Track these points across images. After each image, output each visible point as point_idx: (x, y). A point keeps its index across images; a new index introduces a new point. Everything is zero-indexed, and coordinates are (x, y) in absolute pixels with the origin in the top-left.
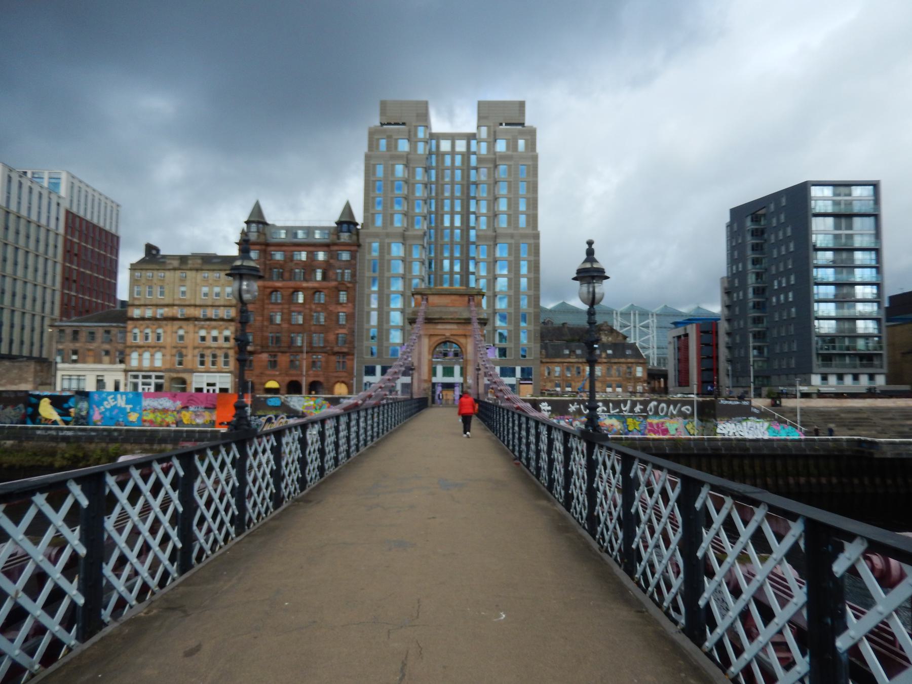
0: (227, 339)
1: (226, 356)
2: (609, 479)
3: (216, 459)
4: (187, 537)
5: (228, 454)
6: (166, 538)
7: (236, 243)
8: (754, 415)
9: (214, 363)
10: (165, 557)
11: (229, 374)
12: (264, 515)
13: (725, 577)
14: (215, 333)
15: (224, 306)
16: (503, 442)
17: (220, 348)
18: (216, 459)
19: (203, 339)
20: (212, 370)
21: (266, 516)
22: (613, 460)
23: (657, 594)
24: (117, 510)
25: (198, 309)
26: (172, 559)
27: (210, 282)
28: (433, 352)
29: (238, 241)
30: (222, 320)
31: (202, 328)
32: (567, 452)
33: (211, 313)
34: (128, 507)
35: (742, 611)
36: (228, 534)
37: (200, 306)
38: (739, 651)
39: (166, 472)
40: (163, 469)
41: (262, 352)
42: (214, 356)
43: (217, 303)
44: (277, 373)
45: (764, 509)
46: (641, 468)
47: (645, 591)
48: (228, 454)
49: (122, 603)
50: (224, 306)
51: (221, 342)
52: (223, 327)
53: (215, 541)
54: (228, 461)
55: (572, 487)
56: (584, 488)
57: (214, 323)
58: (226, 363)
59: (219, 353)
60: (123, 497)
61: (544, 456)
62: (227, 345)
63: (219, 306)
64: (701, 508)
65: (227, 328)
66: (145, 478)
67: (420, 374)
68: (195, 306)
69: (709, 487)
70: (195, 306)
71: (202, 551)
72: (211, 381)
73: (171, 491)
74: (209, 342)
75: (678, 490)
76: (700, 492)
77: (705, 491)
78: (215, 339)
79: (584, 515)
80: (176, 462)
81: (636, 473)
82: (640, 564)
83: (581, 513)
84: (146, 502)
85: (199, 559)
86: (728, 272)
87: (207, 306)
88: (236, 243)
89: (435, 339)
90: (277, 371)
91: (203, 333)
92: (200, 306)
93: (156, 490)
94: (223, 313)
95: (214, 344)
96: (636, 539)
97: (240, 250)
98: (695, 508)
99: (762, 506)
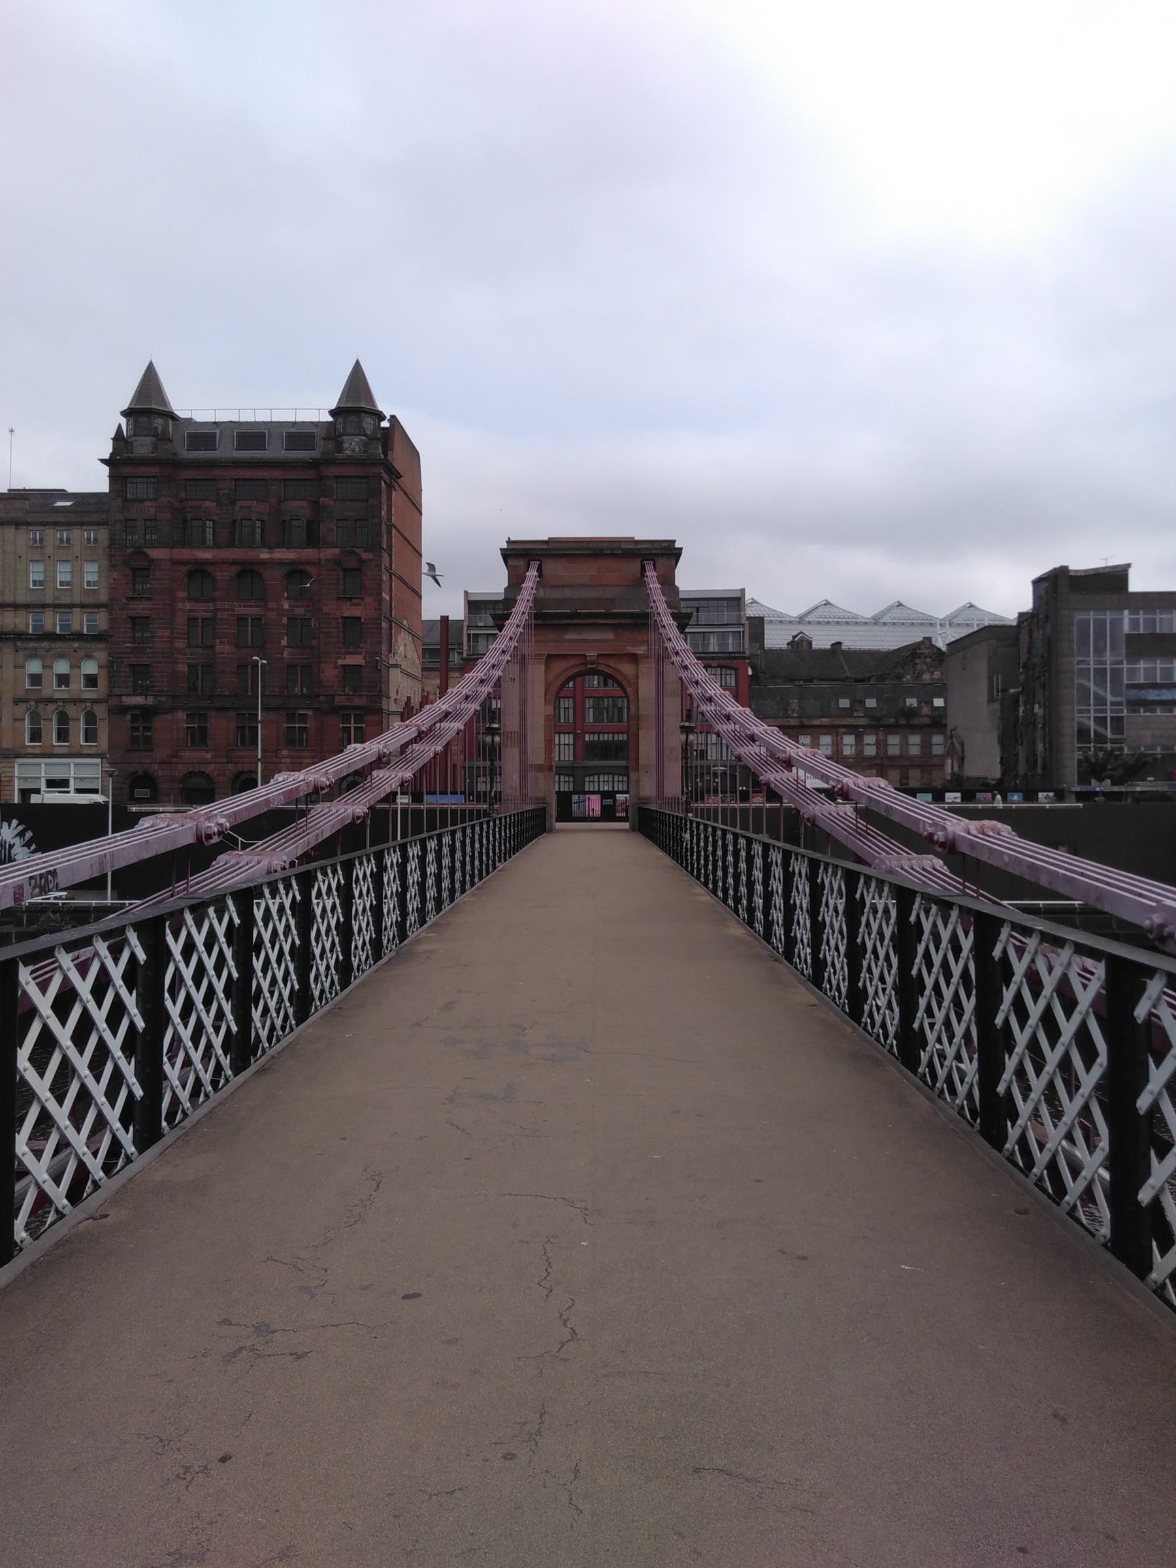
0: (91, 681)
1: (91, 718)
2: (945, 960)
3: (220, 921)
4: (152, 1077)
5: (199, 927)
6: (117, 1077)
7: (103, 461)
8: (221, 848)
9: (63, 735)
10: (113, 1115)
11: (98, 761)
12: (267, 1045)
13: (952, 1001)
14: (62, 667)
15: (82, 606)
16: (714, 891)
17: (75, 701)
18: (220, 921)
19: (36, 679)
20: (57, 751)
21: (270, 1047)
22: (885, 901)
23: (949, 1094)
24: (35, 1029)
25: (22, 612)
26: (125, 1120)
27: (49, 550)
28: (555, 695)
29: (107, 457)
30: (79, 637)
31: (34, 655)
32: (816, 892)
33: (53, 622)
34: (54, 1023)
35: (1027, 1075)
36: (219, 1068)
37: (27, 606)
38: (1076, 1171)
39: (116, 952)
40: (110, 948)
41: (172, 710)
42: (63, 718)
43: (66, 600)
44: (209, 756)
45: (1070, 949)
46: (1014, 945)
47: (932, 1088)
48: (199, 927)
49: (43, 1200)
50: (82, 606)
51: (78, 687)
52: (82, 653)
53: (198, 1083)
54: (221, 931)
55: (824, 947)
56: (842, 949)
57: (58, 646)
58: (90, 735)
59: (71, 710)
60: (44, 1003)
61: (803, 918)
62: (90, 693)
63: (71, 606)
64: (1000, 959)
65: (89, 657)
66: (83, 969)
67: (523, 752)
68: (16, 606)
69: (1164, 981)
70: (16, 606)
71: (175, 1100)
72: (58, 775)
73: (124, 992)
74: (51, 688)
75: (1095, 985)
76: (1142, 989)
77: (1155, 987)
78: (63, 680)
79: (844, 990)
80: (132, 937)
81: (1005, 952)
82: (924, 1051)
83: (838, 989)
84: (85, 1014)
85: (171, 1117)
86: (1076, 571)
87: (44, 606)
88: (103, 461)
89: (559, 667)
90: (207, 751)
91: (34, 667)
92: (27, 606)
93: (100, 988)
94: (80, 622)
95: (62, 693)
96: (919, 1014)
97: (112, 477)
98: (1134, 1019)
99: (1067, 946)
